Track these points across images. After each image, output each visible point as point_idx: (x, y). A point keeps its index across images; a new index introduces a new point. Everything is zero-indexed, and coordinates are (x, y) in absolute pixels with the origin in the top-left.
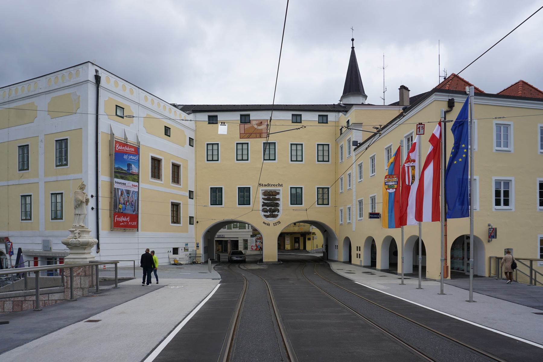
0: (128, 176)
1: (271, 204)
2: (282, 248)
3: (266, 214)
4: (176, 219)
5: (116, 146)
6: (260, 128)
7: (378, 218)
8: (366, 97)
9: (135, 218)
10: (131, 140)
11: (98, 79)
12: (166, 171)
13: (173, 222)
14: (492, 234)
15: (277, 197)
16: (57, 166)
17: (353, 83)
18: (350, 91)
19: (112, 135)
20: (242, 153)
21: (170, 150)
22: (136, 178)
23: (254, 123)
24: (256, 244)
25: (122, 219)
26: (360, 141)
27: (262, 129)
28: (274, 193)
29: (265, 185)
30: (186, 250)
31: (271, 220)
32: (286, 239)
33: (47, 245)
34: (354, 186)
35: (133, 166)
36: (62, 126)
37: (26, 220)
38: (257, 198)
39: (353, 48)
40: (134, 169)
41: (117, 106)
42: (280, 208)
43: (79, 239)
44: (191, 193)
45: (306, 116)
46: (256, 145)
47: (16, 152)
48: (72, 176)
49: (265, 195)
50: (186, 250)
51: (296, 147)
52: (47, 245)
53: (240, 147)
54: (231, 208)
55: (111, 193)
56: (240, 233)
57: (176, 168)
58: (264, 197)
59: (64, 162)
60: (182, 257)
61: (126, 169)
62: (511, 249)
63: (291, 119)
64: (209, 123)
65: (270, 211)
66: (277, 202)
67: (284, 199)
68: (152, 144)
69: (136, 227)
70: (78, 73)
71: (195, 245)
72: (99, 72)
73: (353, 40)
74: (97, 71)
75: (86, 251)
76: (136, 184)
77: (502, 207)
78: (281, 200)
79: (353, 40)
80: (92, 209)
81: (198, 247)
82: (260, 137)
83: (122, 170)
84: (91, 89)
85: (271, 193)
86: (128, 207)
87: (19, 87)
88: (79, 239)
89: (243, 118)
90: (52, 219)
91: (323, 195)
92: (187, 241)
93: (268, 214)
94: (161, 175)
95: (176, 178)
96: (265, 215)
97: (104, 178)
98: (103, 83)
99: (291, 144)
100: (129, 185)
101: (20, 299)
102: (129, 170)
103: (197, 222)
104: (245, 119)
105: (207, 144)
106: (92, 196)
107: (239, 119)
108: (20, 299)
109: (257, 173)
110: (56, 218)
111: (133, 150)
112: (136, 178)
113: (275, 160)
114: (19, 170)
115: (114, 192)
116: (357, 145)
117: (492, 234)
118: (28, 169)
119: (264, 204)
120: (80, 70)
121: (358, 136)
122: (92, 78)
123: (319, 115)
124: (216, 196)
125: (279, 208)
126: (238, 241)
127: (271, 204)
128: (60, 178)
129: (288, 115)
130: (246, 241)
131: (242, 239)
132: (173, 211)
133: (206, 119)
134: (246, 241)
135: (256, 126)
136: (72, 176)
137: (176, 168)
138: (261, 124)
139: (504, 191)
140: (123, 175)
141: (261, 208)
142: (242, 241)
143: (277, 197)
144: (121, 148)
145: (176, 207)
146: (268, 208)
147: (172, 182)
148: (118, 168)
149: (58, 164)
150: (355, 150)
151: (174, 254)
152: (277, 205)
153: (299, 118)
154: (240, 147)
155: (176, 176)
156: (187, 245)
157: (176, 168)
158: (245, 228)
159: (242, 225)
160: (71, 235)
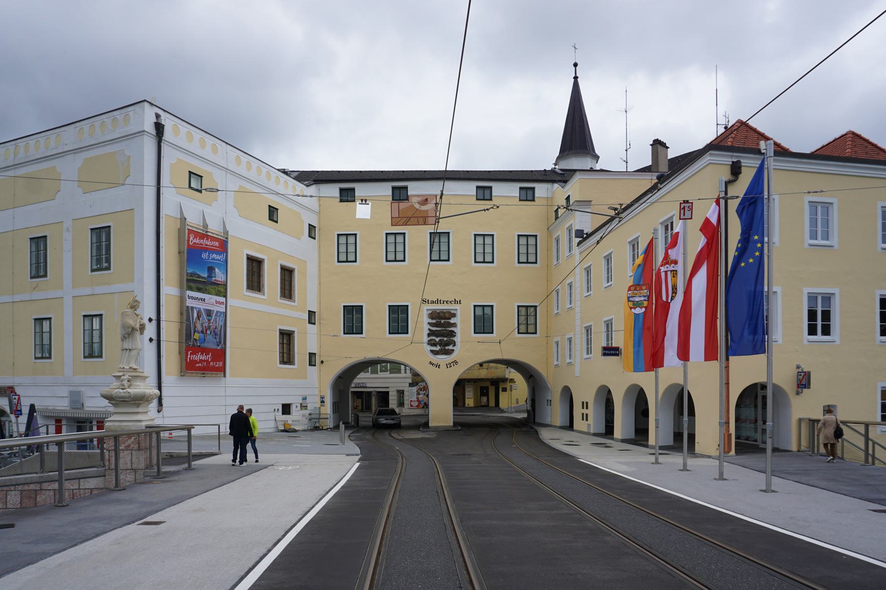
0: (209, 287)
1: (442, 332)
2: (460, 404)
3: (434, 348)
4: (287, 357)
5: (189, 238)
6: (424, 208)
7: (617, 355)
8: (597, 158)
9: (220, 355)
10: (214, 228)
11: (159, 128)
12: (271, 278)
13: (283, 362)
14: (803, 381)
15: (452, 321)
16: (92, 271)
17: (577, 136)
18: (570, 149)
19: (183, 219)
20: (395, 249)
21: (278, 245)
22: (222, 290)
23: (414, 200)
24: (418, 398)
25: (199, 357)
26: (588, 230)
27: (427, 211)
28: (447, 315)
29: (433, 302)
30: (303, 407)
31: (442, 359)
32: (467, 390)
33: (76, 399)
34: (578, 303)
35: (217, 270)
36: (101, 205)
37: (42, 358)
38: (420, 323)
39: (576, 78)
40: (219, 276)
41: (190, 172)
42: (457, 339)
43: (129, 390)
44: (311, 314)
45: (499, 189)
46: (418, 237)
47: (26, 248)
48: (117, 287)
49: (432, 318)
50: (303, 407)
51: (484, 239)
52: (76, 399)
53: (391, 239)
54: (377, 340)
55: (181, 314)
56: (392, 380)
57: (287, 273)
58: (431, 321)
59: (105, 265)
60: (297, 418)
61: (205, 275)
62: (835, 406)
63: (475, 194)
64: (341, 201)
65: (441, 343)
66: (452, 329)
67: (463, 324)
68: (248, 235)
69: (223, 370)
70: (127, 118)
71: (318, 400)
72: (162, 118)
73: (576, 65)
74: (158, 116)
75: (140, 410)
76: (222, 299)
77: (819, 337)
78: (459, 325)
79: (576, 65)
80: (151, 340)
81: (322, 402)
82: (425, 224)
83: (199, 276)
84: (149, 145)
85: (441, 315)
86: (210, 338)
87: (32, 141)
88: (129, 390)
89: (397, 192)
90: (85, 357)
91: (527, 318)
92: (305, 393)
93: (438, 348)
94: (263, 285)
95: (287, 291)
96: (432, 351)
97: (170, 291)
98: (168, 135)
99: (475, 235)
100: (211, 301)
101: (32, 487)
102: (210, 276)
103: (322, 362)
104: (400, 195)
105: (338, 235)
106: (150, 320)
107: (390, 193)
108: (32, 487)
109: (419, 283)
110: (91, 355)
111: (217, 244)
112: (222, 290)
113: (448, 260)
114: (32, 278)
115: (185, 313)
116: (583, 236)
117: (803, 381)
118: (45, 276)
119: (431, 333)
120: (131, 114)
121: (583, 221)
122: (150, 128)
123: (521, 188)
124: (353, 319)
125: (455, 339)
126: (388, 393)
127: (442, 332)
128: (99, 290)
129: (470, 188)
130: (401, 393)
131: (394, 389)
132: (282, 344)
133: (337, 194)
134: (401, 393)
135: (417, 206)
136: (117, 287)
137: (287, 274)
138: (425, 201)
139: (822, 311)
140: (200, 286)
141: (426, 339)
142: (395, 393)
143: (452, 321)
144: (197, 241)
145: (287, 337)
146: (437, 340)
147: (281, 296)
148: (192, 275)
149: (95, 267)
150: (579, 244)
151: (283, 413)
152: (452, 334)
153: (487, 192)
154: (391, 239)
155: (287, 287)
156: (305, 399)
157: (287, 274)
158: (399, 371)
159: (395, 366)
160: (116, 383)
